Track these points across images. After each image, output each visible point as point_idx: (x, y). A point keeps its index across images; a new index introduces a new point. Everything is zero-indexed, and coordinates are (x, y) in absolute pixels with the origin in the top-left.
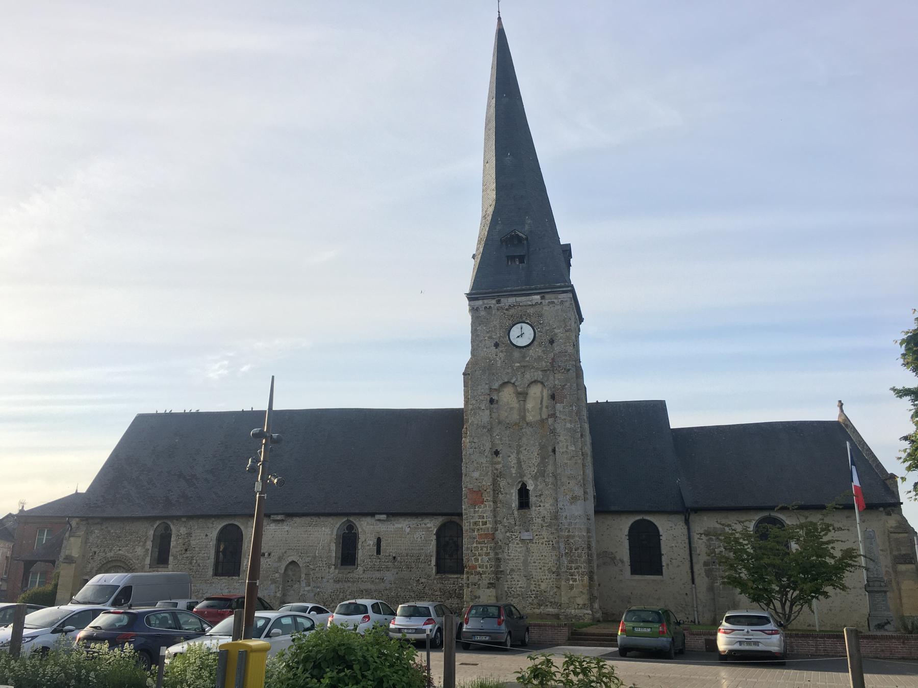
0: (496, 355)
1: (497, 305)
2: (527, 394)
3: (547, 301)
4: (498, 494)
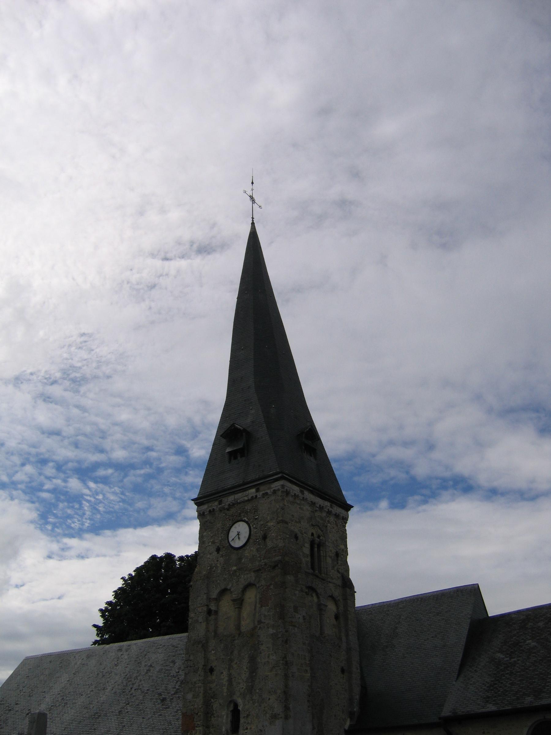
0: (217, 561)
1: (219, 506)
2: (243, 600)
3: (261, 493)
4: (211, 717)
